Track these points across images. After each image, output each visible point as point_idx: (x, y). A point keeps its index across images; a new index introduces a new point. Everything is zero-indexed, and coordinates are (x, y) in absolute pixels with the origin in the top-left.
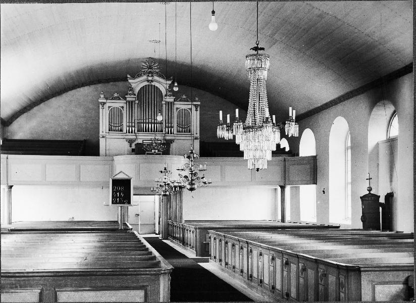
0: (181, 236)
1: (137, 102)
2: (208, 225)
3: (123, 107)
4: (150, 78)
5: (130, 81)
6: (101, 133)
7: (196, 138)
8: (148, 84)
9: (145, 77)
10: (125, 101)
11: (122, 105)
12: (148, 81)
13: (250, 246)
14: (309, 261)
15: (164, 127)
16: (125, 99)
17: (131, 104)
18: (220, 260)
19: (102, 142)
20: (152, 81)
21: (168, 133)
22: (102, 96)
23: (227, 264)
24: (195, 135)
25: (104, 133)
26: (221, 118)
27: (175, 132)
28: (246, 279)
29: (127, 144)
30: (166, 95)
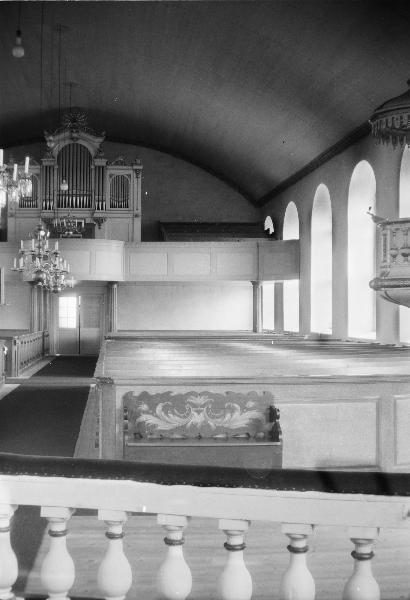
4: (75, 135)
7: (136, 216)
9: (67, 134)
10: (38, 167)
11: (127, 172)
12: (72, 139)
16: (40, 163)
20: (77, 139)
24: (136, 212)
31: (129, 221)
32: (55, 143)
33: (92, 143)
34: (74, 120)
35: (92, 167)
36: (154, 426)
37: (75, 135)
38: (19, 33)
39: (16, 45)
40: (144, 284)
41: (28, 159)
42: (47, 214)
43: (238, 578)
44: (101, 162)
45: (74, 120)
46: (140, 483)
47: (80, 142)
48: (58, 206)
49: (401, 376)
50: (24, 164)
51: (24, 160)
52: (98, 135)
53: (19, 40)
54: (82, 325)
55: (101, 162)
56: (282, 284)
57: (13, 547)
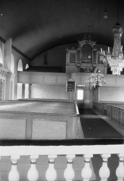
0: (118, 118)
1: (81, 51)
2: (104, 102)
3: (75, 53)
4: (87, 41)
5: (79, 42)
6: (66, 64)
7: (106, 66)
8: (86, 43)
9: (85, 41)
10: (76, 51)
11: (75, 52)
12: (86, 42)
13: (120, 110)
14: (19, 80)
15: (93, 61)
16: (77, 49)
17: (79, 52)
18: (110, 117)
19: (67, 67)
20: (88, 42)
21: (94, 64)
22: (68, 49)
23: (112, 118)
24: (105, 65)
25: (68, 64)
26: (79, 86)
27: (97, 63)
28: (118, 124)
29: (77, 68)
30: (93, 48)
31: (103, 68)
32: (82, 43)
33: (93, 44)
34: (87, 37)
35: (92, 51)
36: (122, 129)
37: (87, 41)
38: (106, 11)
39: (105, 15)
40: (111, 87)
41: (101, 49)
42: (78, 65)
43: (33, 173)
44: (95, 50)
45: (87, 37)
46: (92, 146)
47: (89, 43)
48: (82, 63)
49: (10, 111)
50: (108, 50)
51: (100, 50)
52: (94, 41)
53: (106, 13)
54: (85, 99)
55: (95, 50)
56: (25, 84)
57: (102, 165)
